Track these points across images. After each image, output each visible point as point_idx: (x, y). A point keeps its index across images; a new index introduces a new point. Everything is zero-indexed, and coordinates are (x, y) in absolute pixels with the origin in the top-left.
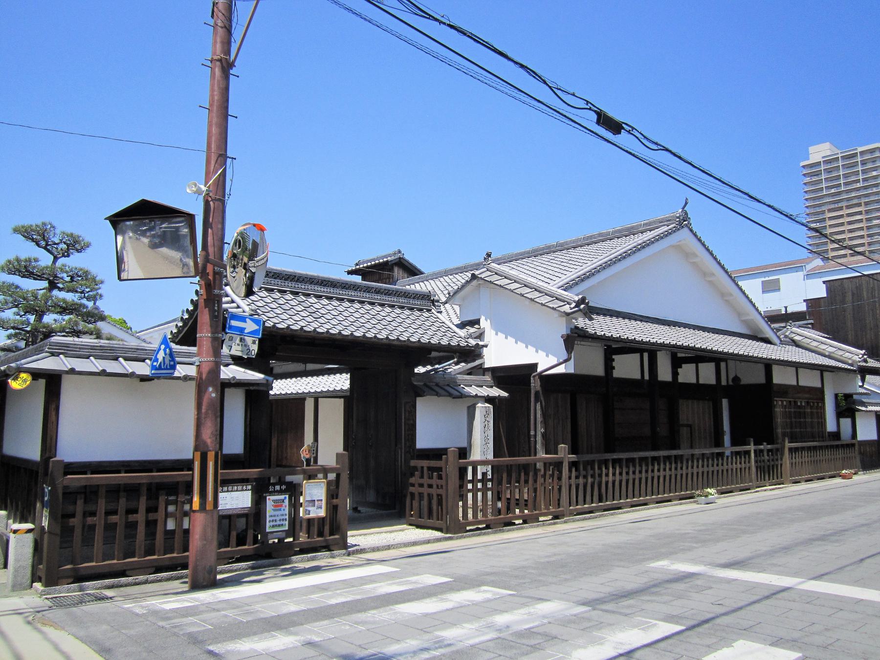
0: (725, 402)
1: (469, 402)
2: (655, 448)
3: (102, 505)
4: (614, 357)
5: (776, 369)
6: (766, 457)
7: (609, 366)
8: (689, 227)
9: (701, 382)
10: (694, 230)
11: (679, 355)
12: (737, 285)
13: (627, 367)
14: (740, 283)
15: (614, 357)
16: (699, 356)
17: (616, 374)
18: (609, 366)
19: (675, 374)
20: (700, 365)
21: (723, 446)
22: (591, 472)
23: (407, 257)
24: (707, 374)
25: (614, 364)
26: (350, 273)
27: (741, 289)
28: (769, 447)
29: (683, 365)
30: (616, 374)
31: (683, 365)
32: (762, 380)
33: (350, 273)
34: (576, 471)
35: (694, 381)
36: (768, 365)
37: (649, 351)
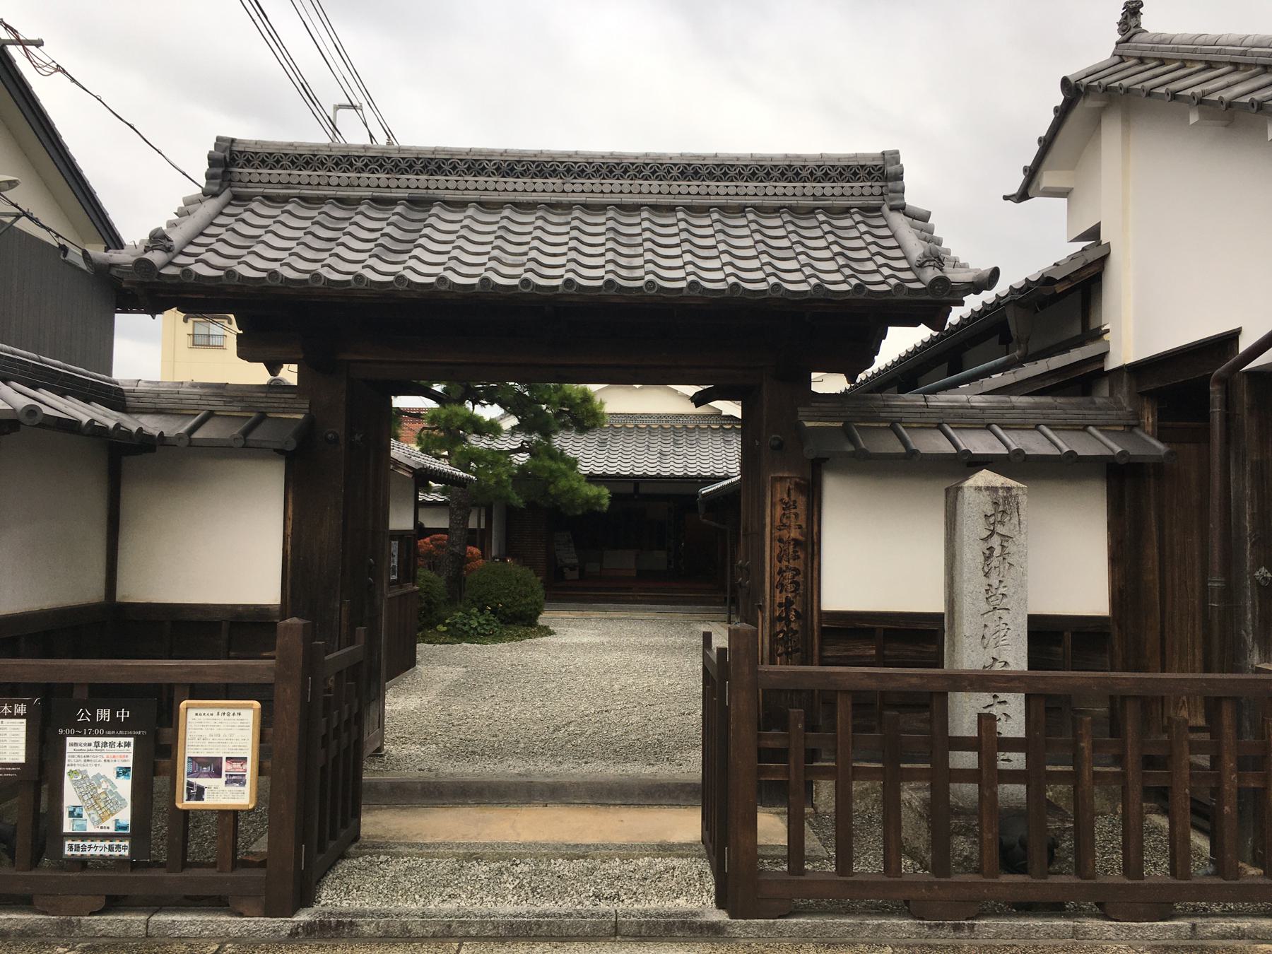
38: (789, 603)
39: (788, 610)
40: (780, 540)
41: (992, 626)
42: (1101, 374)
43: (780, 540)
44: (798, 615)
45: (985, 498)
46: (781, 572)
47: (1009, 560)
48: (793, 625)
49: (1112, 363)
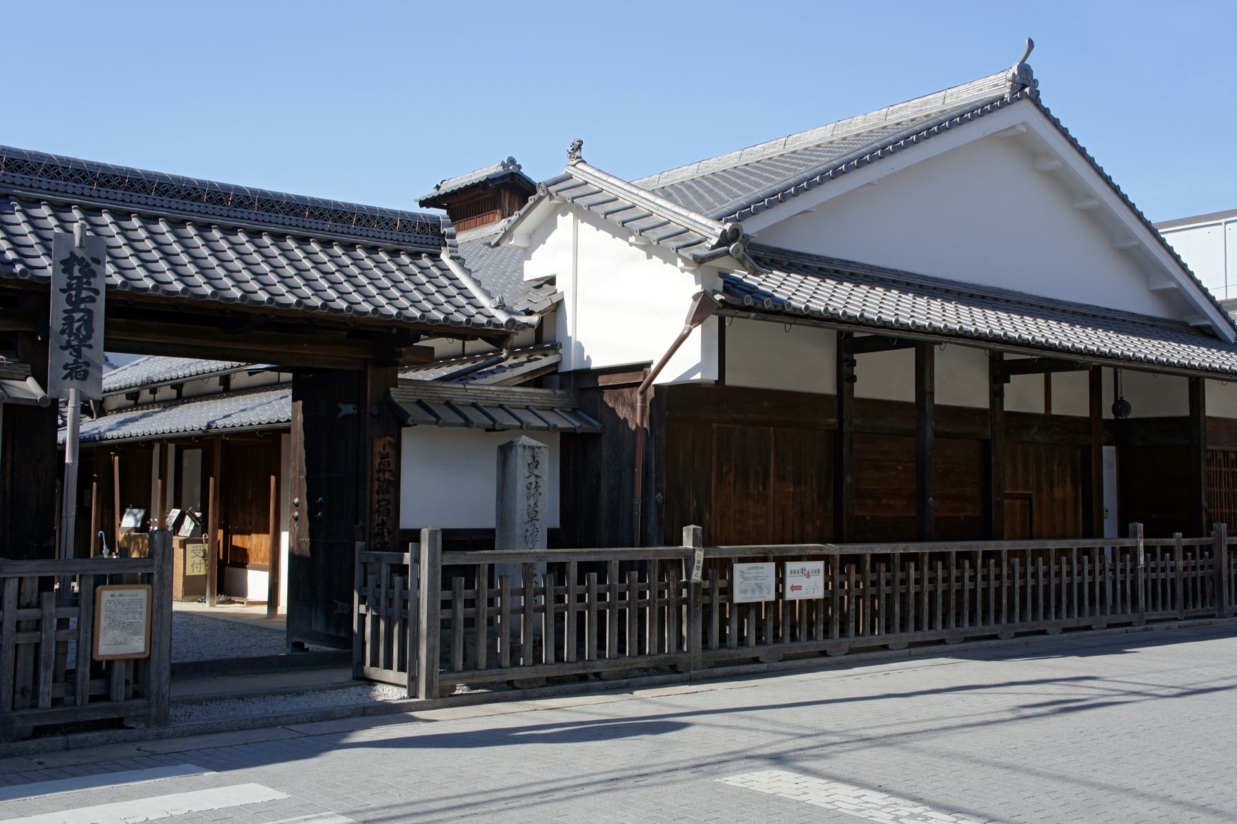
0: (1109, 453)
1: (502, 439)
2: (921, 538)
3: (652, 577)
4: (856, 356)
5: (1212, 389)
6: (1181, 563)
7: (845, 376)
8: (1035, 100)
9: (1055, 411)
10: (1045, 104)
11: (1007, 357)
12: (1162, 242)
13: (885, 378)
14: (1170, 239)
15: (856, 356)
16: (1049, 361)
17: (861, 390)
18: (845, 376)
19: (997, 395)
20: (1054, 375)
21: (1101, 536)
22: (899, 575)
23: (525, 171)
24: (1070, 396)
25: (857, 371)
26: (423, 203)
27: (1170, 250)
28: (1186, 541)
29: (1012, 377)
30: (861, 390)
31: (1012, 377)
32: (1183, 410)
33: (423, 203)
34: (916, 569)
35: (1042, 411)
36: (1196, 379)
37: (922, 343)
38: (383, 523)
39: (383, 529)
40: (379, 480)
41: (530, 529)
42: (556, 372)
43: (379, 480)
44: (389, 532)
45: (528, 452)
46: (378, 502)
47: (540, 490)
48: (387, 539)
49: (564, 368)
